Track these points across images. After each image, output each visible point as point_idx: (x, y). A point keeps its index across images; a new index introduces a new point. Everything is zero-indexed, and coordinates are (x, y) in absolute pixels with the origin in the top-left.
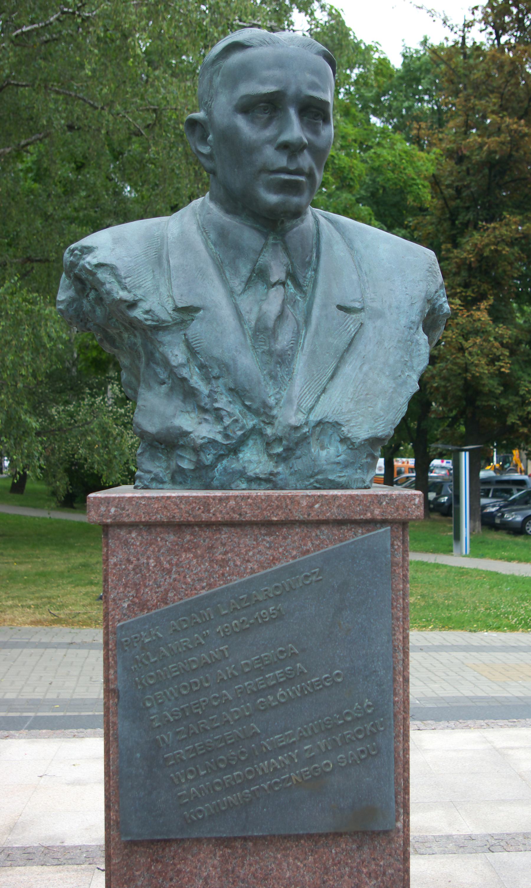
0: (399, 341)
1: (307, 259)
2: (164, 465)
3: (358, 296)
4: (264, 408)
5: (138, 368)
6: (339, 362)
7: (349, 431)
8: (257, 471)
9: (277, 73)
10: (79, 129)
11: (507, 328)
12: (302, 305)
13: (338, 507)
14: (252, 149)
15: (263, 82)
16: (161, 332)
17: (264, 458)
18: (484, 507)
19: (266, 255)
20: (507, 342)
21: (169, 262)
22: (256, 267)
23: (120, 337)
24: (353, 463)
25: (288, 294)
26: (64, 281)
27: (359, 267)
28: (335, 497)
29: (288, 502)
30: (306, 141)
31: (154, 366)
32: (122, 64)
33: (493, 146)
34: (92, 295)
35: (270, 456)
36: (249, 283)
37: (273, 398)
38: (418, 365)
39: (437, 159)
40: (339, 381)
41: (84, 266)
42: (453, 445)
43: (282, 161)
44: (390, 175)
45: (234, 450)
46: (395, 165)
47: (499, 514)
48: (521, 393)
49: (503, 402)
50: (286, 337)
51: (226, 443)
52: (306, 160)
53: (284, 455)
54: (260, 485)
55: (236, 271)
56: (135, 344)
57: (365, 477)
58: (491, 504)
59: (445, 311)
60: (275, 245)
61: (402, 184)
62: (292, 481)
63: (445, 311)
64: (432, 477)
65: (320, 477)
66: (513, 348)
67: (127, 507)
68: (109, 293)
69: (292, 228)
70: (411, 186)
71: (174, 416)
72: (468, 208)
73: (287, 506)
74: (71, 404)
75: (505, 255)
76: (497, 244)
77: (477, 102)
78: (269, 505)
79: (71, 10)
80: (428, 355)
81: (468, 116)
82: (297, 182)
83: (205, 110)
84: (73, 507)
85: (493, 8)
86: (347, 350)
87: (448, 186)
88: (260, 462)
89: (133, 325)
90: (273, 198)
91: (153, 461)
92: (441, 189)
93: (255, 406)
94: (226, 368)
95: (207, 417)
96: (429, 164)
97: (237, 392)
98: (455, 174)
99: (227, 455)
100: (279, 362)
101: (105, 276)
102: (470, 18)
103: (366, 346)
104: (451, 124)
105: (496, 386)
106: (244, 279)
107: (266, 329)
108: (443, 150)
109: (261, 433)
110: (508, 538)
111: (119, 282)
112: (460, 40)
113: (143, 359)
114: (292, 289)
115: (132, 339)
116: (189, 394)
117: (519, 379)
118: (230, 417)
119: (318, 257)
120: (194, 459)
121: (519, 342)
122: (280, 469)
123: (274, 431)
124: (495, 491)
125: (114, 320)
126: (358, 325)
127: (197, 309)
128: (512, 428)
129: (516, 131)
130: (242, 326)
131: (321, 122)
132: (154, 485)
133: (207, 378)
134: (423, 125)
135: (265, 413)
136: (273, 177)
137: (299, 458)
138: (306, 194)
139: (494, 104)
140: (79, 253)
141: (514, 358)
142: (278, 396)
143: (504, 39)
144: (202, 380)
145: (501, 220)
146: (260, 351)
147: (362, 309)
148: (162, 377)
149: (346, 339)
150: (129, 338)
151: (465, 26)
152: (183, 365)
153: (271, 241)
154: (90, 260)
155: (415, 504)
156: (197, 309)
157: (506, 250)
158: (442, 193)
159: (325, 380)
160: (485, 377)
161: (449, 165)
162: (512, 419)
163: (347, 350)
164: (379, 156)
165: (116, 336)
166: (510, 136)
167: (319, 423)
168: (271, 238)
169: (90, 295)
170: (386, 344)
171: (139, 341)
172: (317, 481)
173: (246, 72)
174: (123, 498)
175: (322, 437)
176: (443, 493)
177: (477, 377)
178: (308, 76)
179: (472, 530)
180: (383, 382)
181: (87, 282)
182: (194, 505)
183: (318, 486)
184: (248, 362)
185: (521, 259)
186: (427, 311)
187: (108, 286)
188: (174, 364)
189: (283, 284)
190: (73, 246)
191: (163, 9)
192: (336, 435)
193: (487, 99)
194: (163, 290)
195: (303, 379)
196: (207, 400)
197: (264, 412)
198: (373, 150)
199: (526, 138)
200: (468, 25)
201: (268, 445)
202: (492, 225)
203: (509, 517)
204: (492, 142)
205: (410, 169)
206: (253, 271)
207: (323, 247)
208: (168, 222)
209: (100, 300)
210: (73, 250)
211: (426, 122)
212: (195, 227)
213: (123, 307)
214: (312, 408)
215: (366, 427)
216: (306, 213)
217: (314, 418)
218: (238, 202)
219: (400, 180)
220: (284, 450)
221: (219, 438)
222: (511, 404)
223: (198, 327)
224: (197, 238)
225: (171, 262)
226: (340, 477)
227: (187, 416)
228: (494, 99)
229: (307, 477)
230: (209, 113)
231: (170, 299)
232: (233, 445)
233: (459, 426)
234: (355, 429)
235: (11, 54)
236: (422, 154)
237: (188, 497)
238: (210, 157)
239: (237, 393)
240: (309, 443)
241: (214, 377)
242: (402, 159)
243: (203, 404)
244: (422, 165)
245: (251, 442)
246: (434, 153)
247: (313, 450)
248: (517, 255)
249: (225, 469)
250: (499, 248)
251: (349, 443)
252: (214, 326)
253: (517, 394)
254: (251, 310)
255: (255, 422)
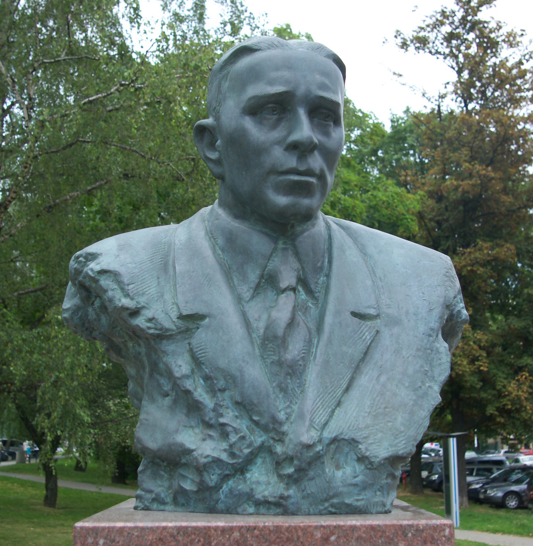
0: (418, 350)
1: (319, 265)
2: (166, 484)
3: (373, 302)
4: (273, 424)
5: (142, 378)
6: (355, 372)
7: (367, 449)
8: (266, 493)
9: (286, 74)
10: (133, 177)
11: (484, 334)
12: (314, 311)
13: (357, 539)
14: (260, 151)
15: (271, 83)
16: (164, 341)
17: (274, 479)
18: (470, 484)
19: (276, 259)
20: (484, 345)
21: (175, 268)
22: (265, 273)
23: (126, 346)
24: (372, 485)
25: (299, 300)
26: (70, 289)
27: (373, 272)
28: (353, 528)
29: (300, 533)
30: (316, 141)
31: (158, 377)
32: (167, 124)
33: (466, 188)
34: (97, 303)
35: (280, 476)
36: (257, 289)
37: (283, 413)
38: (440, 375)
39: (421, 199)
40: (355, 393)
41: (87, 273)
42: (442, 432)
43: (292, 162)
44: (385, 212)
45: (241, 469)
46: (389, 204)
47: (483, 490)
48: (498, 387)
49: (483, 395)
50: (297, 346)
51: (231, 462)
52: (316, 162)
53: (295, 476)
54: (269, 509)
55: (244, 277)
56: (139, 353)
57: (385, 500)
58: (475, 482)
59: (464, 317)
60: (284, 249)
61: (395, 219)
62: (305, 505)
63: (464, 317)
64: (424, 458)
65: (335, 501)
66: (489, 350)
67: (117, 539)
68: (111, 300)
69: (303, 232)
70: (401, 220)
71: (177, 431)
72: (447, 237)
73: (298, 538)
74: (127, 397)
75: (479, 274)
76: (472, 265)
77: (451, 155)
78: (278, 537)
79: (127, 83)
80: (449, 364)
81: (445, 165)
82: (308, 183)
83: (213, 116)
84: (125, 483)
85: (461, 83)
86: (363, 360)
87: (430, 220)
88: (269, 484)
89: (137, 334)
90: (282, 201)
91: (155, 479)
92: (425, 223)
93: (263, 422)
94: (233, 380)
95: (211, 433)
96: (416, 203)
97: (245, 406)
98: (436, 210)
99: (233, 475)
100: (290, 374)
101: (107, 282)
102: (443, 91)
103: (383, 355)
104: (431, 171)
105: (476, 382)
106: (253, 285)
107: (276, 337)
108: (426, 192)
109: (271, 451)
110: (491, 511)
111: (122, 289)
112: (437, 108)
113: (147, 370)
114: (303, 295)
115: (137, 348)
116: (193, 408)
117: (495, 375)
118: (237, 434)
119: (330, 262)
120: (197, 480)
121: (494, 345)
122: (291, 492)
123: (284, 449)
124: (478, 470)
125: (119, 329)
126: (373, 333)
127: (202, 317)
128: (491, 418)
129: (484, 176)
130: (250, 334)
131: (332, 124)
132: (155, 506)
133: (213, 391)
134: (409, 173)
135: (274, 429)
136: (282, 178)
137: (312, 479)
138: (318, 196)
139: (466, 156)
140: (83, 260)
141: (490, 358)
142: (288, 411)
143: (471, 106)
144: (207, 392)
145: (475, 246)
146: (269, 361)
147: (377, 316)
148: (165, 389)
149: (361, 347)
150: (133, 347)
151: (440, 97)
152: (187, 377)
153: (281, 245)
154: (94, 266)
155: (445, 536)
156: (202, 317)
157: (481, 270)
158: (426, 225)
159: (340, 392)
160: (467, 374)
161: (431, 202)
162: (490, 410)
163: (363, 360)
164: (375, 197)
165: (122, 346)
166: (480, 180)
167: (334, 440)
168: (281, 242)
169: (96, 303)
170: (404, 353)
171: (143, 350)
172: (332, 506)
173: (254, 74)
174: (113, 528)
175: (337, 456)
176: (433, 472)
177: (460, 375)
178: (318, 77)
179: (461, 504)
180: (403, 394)
181: (92, 290)
182: (193, 536)
183: (333, 510)
184: (256, 373)
185: (491, 277)
186: (446, 317)
187: (110, 293)
188: (177, 375)
189: (294, 290)
190: (78, 253)
191: (199, 80)
192: (352, 453)
193: (460, 152)
194: (168, 297)
195: (315, 392)
196: (212, 414)
197: (273, 428)
198: (370, 193)
199: (493, 181)
200: (442, 97)
201: (278, 464)
202: (468, 250)
203: (491, 493)
204: (466, 184)
205: (401, 206)
206: (262, 276)
207: (336, 252)
208: (177, 229)
209: (104, 308)
210: (78, 257)
211: (412, 170)
212: (202, 233)
213: (125, 314)
214: (326, 424)
215: (386, 444)
216: (316, 218)
217: (328, 434)
218: (246, 207)
219: (393, 216)
220: (296, 471)
221: (224, 457)
222: (490, 397)
223: (203, 335)
224: (204, 245)
225: (177, 268)
226: (358, 500)
227: (190, 431)
228: (465, 151)
229: (321, 501)
230: (217, 119)
231: (175, 306)
232: (239, 464)
233: (446, 415)
234: (374, 446)
235: (79, 117)
236: (410, 195)
237: (186, 528)
238: (218, 162)
239: (244, 406)
240: (323, 463)
241: (219, 390)
242: (394, 199)
243: (207, 419)
244: (410, 204)
245: (259, 461)
246: (420, 195)
247: (327, 470)
248: (489, 274)
249: (231, 491)
250: (475, 269)
251: (367, 462)
252: (221, 334)
253: (494, 389)
254: (260, 317)
255: (264, 438)
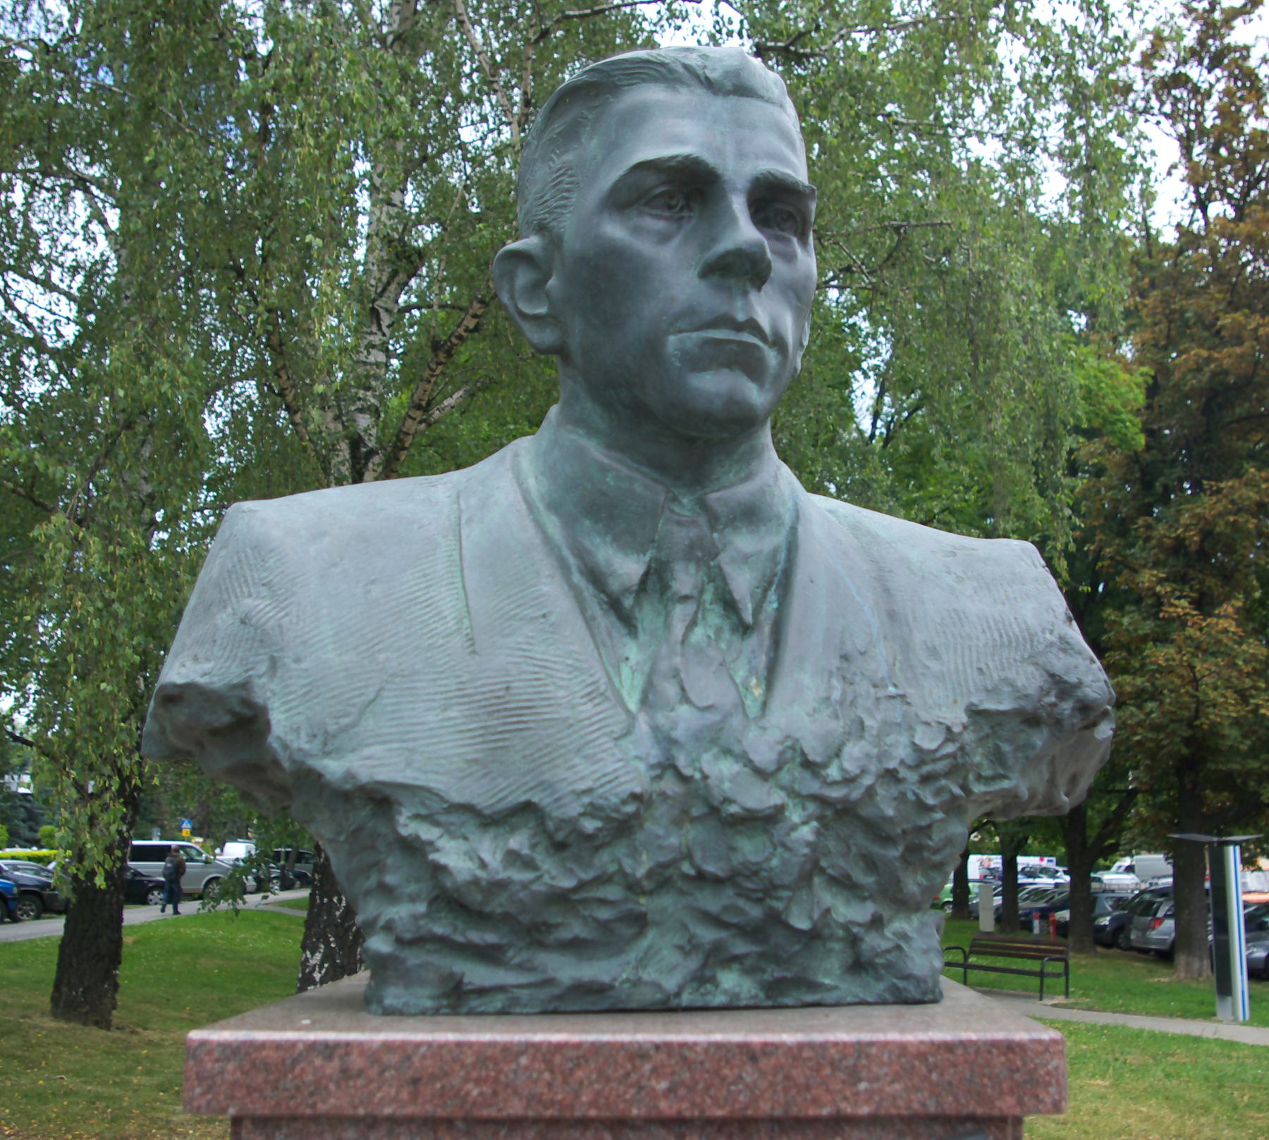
33: (1226, 363)
70: (1113, 423)
